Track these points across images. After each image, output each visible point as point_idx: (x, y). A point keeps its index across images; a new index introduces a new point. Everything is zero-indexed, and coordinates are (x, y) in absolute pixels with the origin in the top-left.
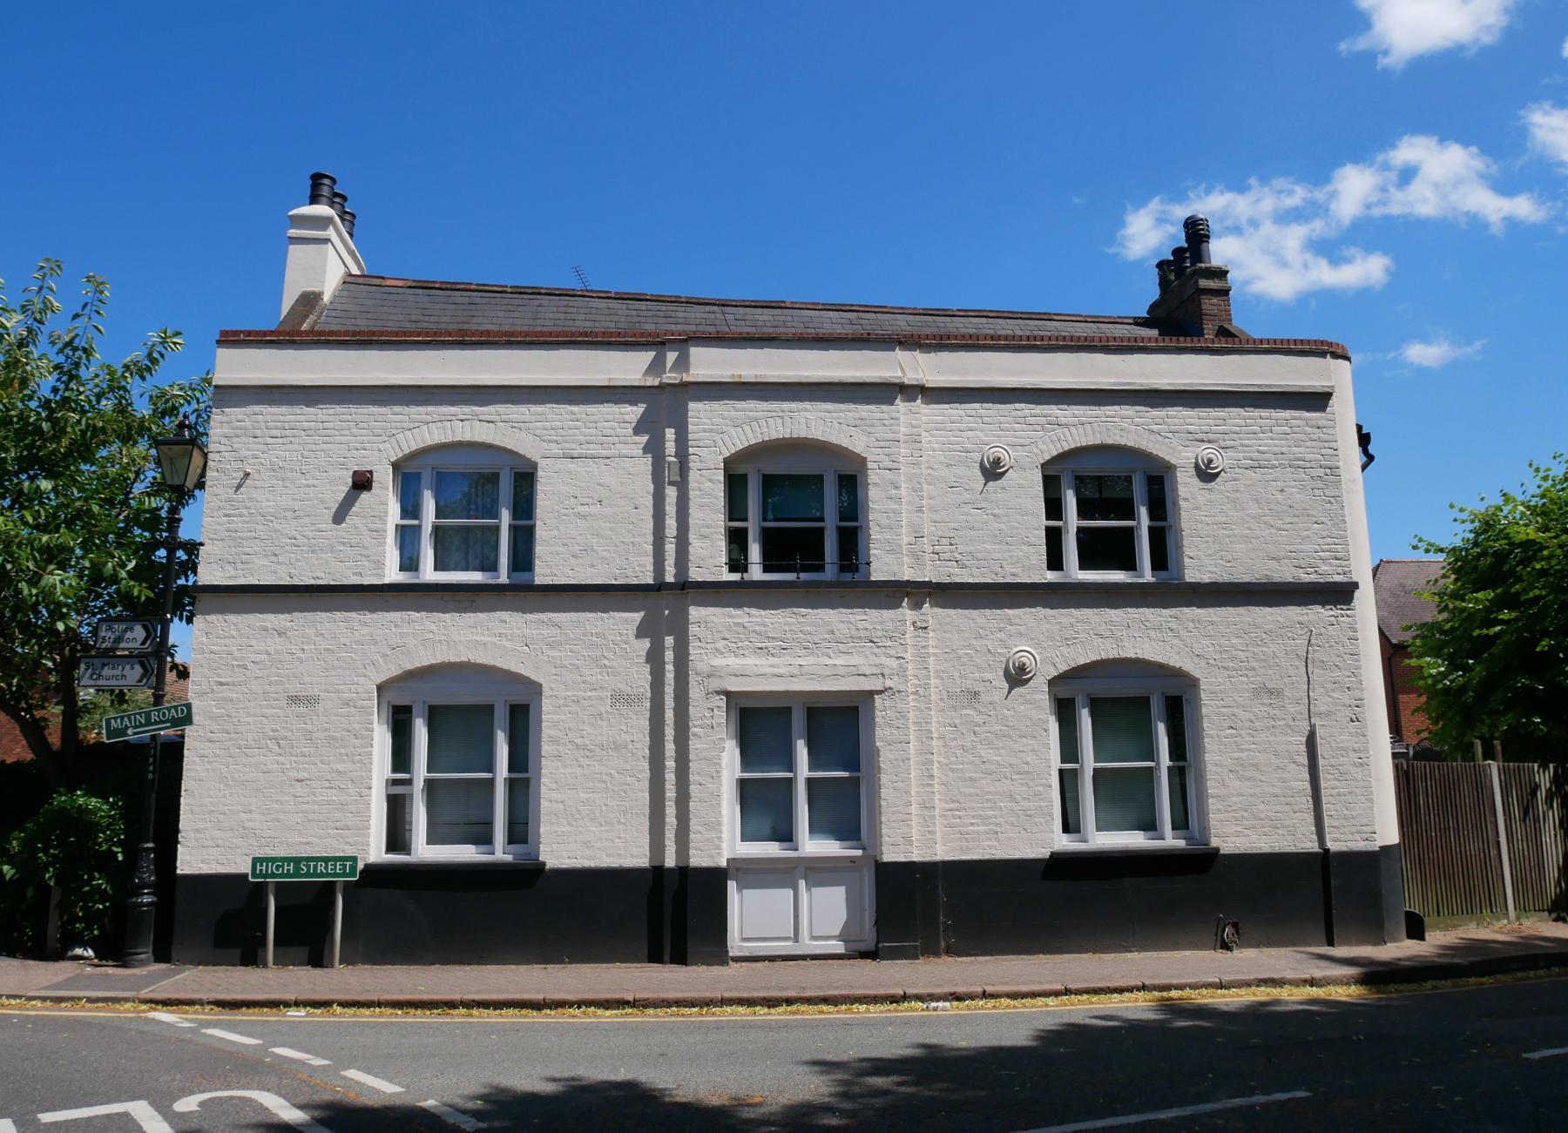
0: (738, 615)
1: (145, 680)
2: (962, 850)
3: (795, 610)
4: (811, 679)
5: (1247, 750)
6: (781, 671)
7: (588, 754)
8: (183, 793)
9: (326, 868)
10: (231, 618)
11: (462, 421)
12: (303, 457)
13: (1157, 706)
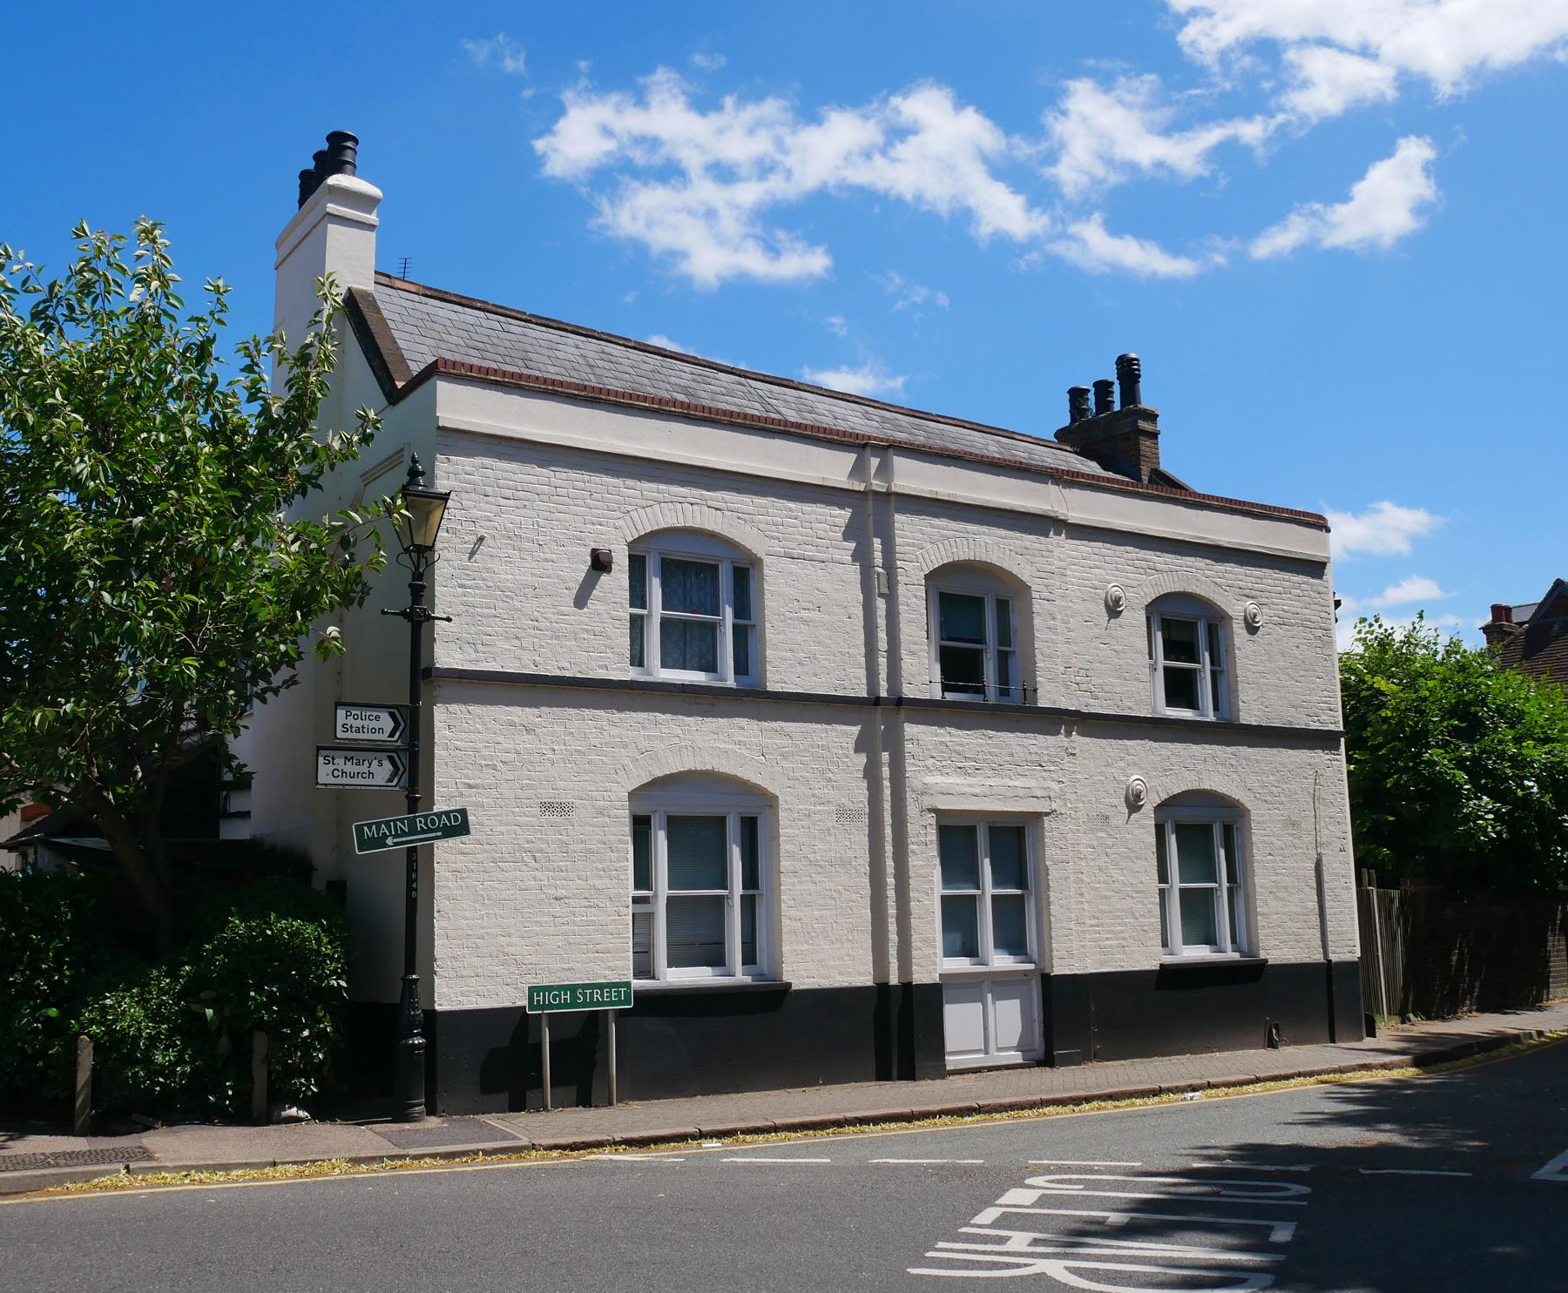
0: (941, 734)
1: (396, 780)
2: (1102, 963)
3: (985, 732)
4: (999, 799)
5: (1281, 874)
6: (977, 790)
7: (820, 870)
8: (436, 915)
9: (602, 996)
10: (476, 709)
11: (692, 504)
12: (538, 526)
13: (733, 829)
